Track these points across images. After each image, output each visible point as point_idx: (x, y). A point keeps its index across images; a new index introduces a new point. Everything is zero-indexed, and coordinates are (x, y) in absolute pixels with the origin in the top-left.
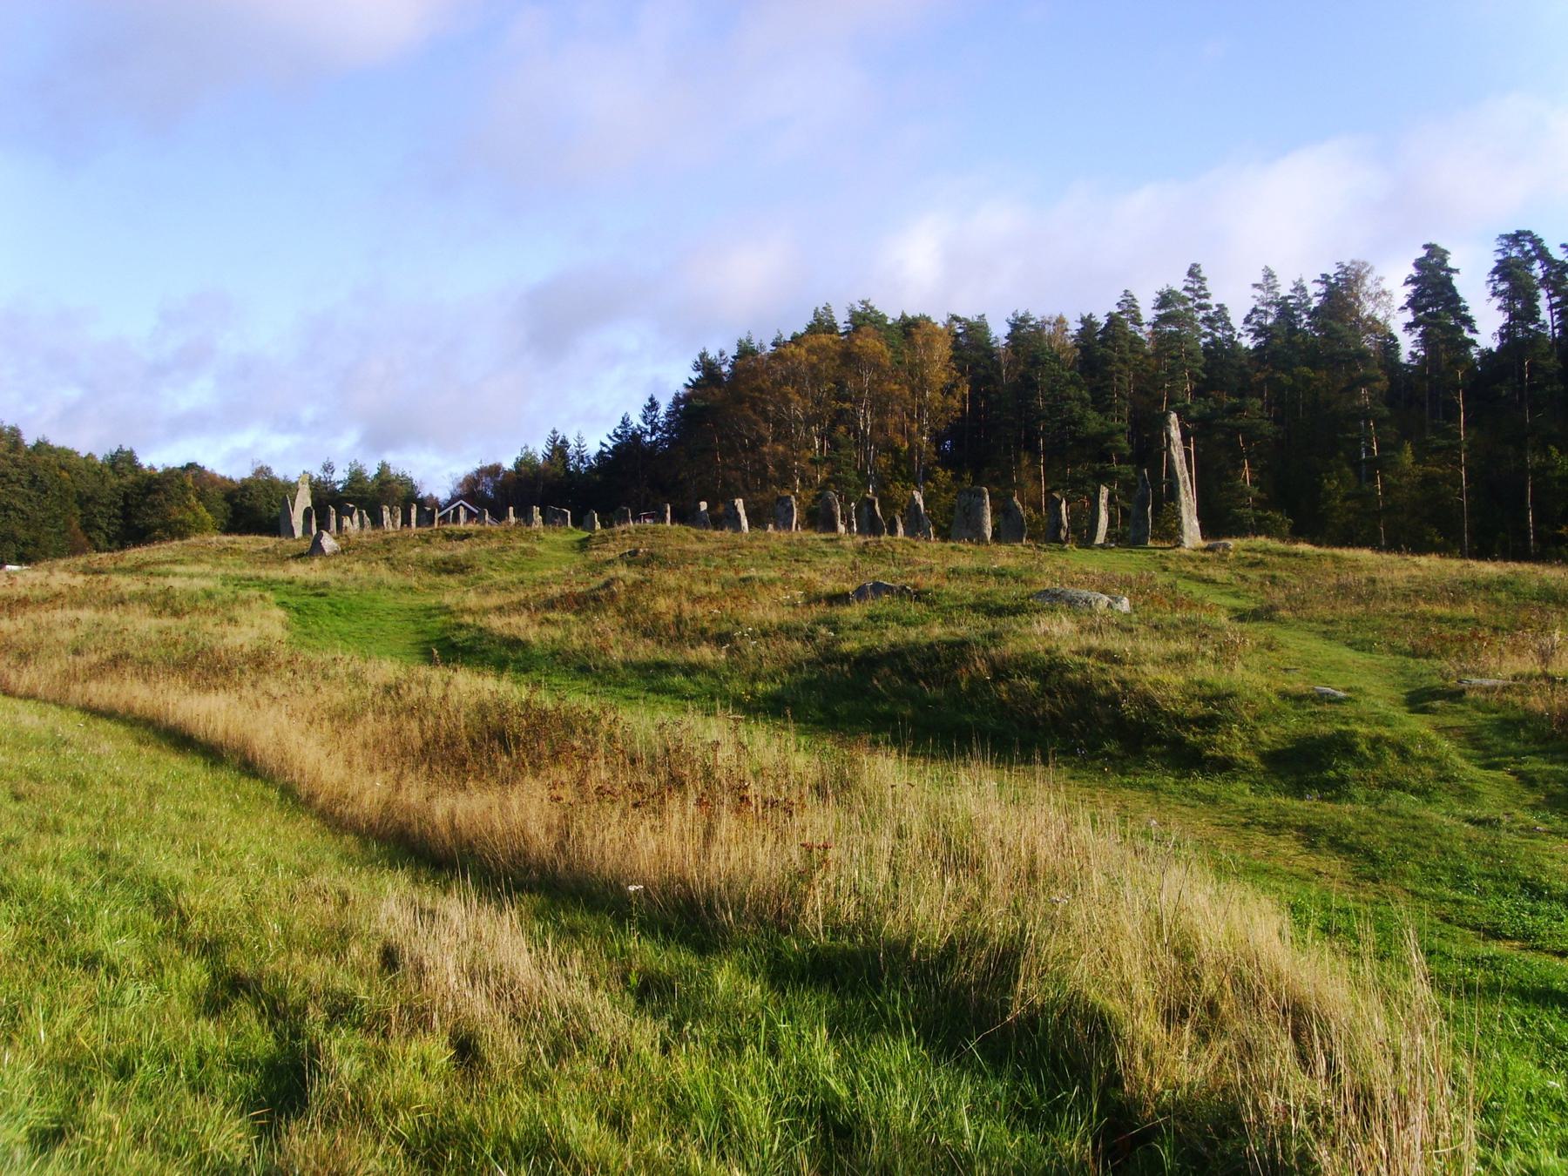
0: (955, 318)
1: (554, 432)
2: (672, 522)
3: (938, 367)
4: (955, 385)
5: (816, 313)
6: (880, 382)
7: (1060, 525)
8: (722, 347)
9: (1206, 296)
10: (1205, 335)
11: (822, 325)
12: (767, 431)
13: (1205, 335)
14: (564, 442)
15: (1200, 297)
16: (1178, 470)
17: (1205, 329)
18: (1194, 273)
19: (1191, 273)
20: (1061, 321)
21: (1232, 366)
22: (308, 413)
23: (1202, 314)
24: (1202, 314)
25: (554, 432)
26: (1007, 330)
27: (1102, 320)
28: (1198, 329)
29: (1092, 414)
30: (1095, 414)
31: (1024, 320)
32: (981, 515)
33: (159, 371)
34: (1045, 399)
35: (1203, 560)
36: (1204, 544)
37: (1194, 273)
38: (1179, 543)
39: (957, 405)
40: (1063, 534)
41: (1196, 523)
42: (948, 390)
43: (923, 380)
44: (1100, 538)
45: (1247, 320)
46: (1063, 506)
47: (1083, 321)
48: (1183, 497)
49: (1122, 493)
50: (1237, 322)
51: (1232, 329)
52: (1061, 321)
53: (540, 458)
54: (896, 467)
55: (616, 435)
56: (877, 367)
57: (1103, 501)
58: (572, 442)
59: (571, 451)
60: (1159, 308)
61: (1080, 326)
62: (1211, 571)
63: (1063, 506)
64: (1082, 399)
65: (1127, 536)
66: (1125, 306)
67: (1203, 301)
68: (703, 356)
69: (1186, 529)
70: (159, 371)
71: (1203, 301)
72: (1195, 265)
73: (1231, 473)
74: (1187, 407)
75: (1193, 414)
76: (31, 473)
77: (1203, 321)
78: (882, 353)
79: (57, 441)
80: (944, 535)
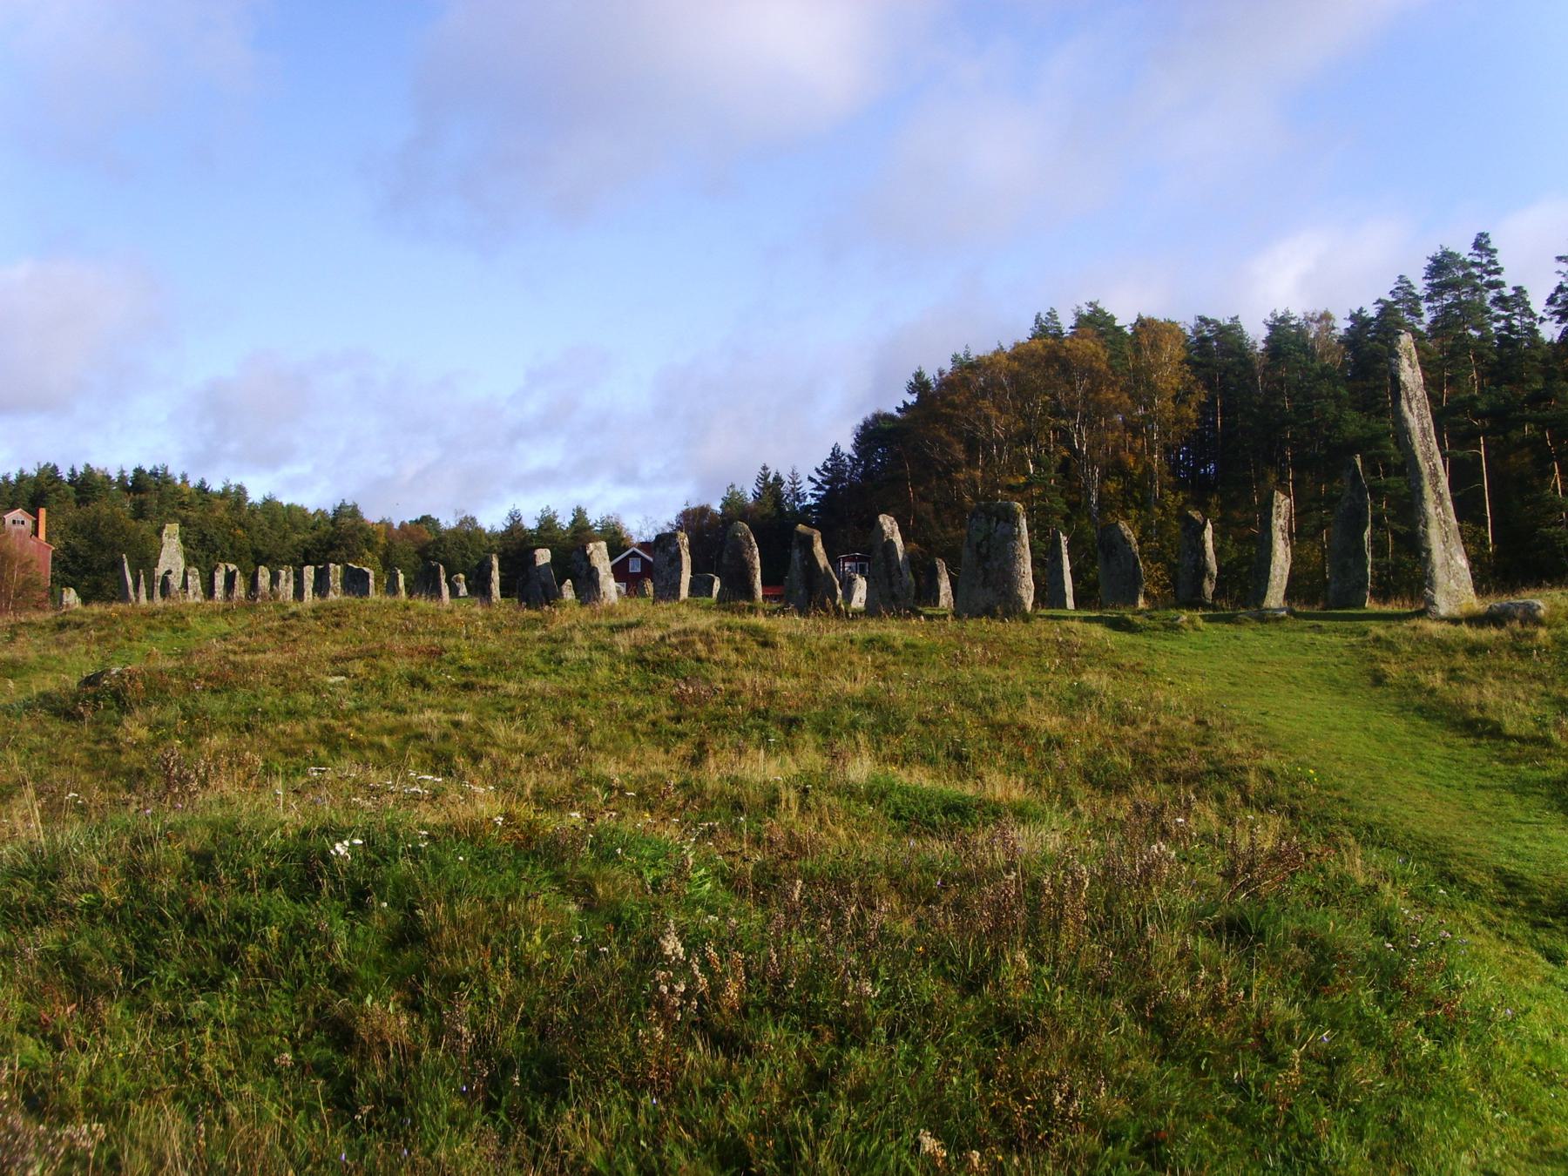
0: (1203, 320)
1: (765, 468)
2: (410, 593)
3: (1169, 375)
4: (1189, 391)
5: (1038, 318)
6: (1095, 389)
7: (1202, 570)
8: (937, 364)
9: (1498, 272)
10: (1497, 318)
11: (1045, 330)
12: (959, 452)
13: (1497, 318)
14: (778, 479)
15: (1490, 273)
16: (1419, 450)
17: (1496, 311)
18: (1481, 244)
19: (1477, 245)
20: (1326, 317)
21: (1533, 358)
22: (647, 468)
23: (1493, 293)
24: (1493, 293)
25: (765, 468)
26: (1265, 332)
27: (1372, 312)
28: (1488, 311)
29: (1350, 415)
30: (1355, 415)
31: (1283, 320)
32: (1011, 560)
33: (519, 433)
34: (1291, 398)
35: (1474, 650)
36: (1477, 605)
37: (1481, 244)
38: (1425, 610)
39: (1192, 415)
40: (1209, 588)
41: (1462, 562)
42: (1180, 398)
43: (1151, 387)
44: (1275, 597)
45: (1551, 301)
46: (1208, 534)
47: (1353, 317)
48: (1430, 508)
49: (1392, 512)
50: (1538, 305)
51: (1532, 315)
52: (1326, 317)
53: (750, 498)
54: (1127, 492)
55: (826, 469)
56: (1091, 372)
57: (1279, 523)
58: (786, 478)
59: (786, 488)
60: (1432, 278)
61: (1349, 324)
62: (1491, 693)
63: (1208, 534)
64: (1337, 397)
65: (1321, 592)
66: (1401, 294)
67: (1494, 278)
68: (919, 375)
69: (1440, 575)
70: (519, 433)
71: (1494, 278)
72: (1483, 235)
73: (1536, 482)
74: (1474, 398)
75: (1481, 406)
76: (201, 531)
77: (1493, 302)
78: (1096, 355)
79: (285, 500)
80: (1106, 585)
